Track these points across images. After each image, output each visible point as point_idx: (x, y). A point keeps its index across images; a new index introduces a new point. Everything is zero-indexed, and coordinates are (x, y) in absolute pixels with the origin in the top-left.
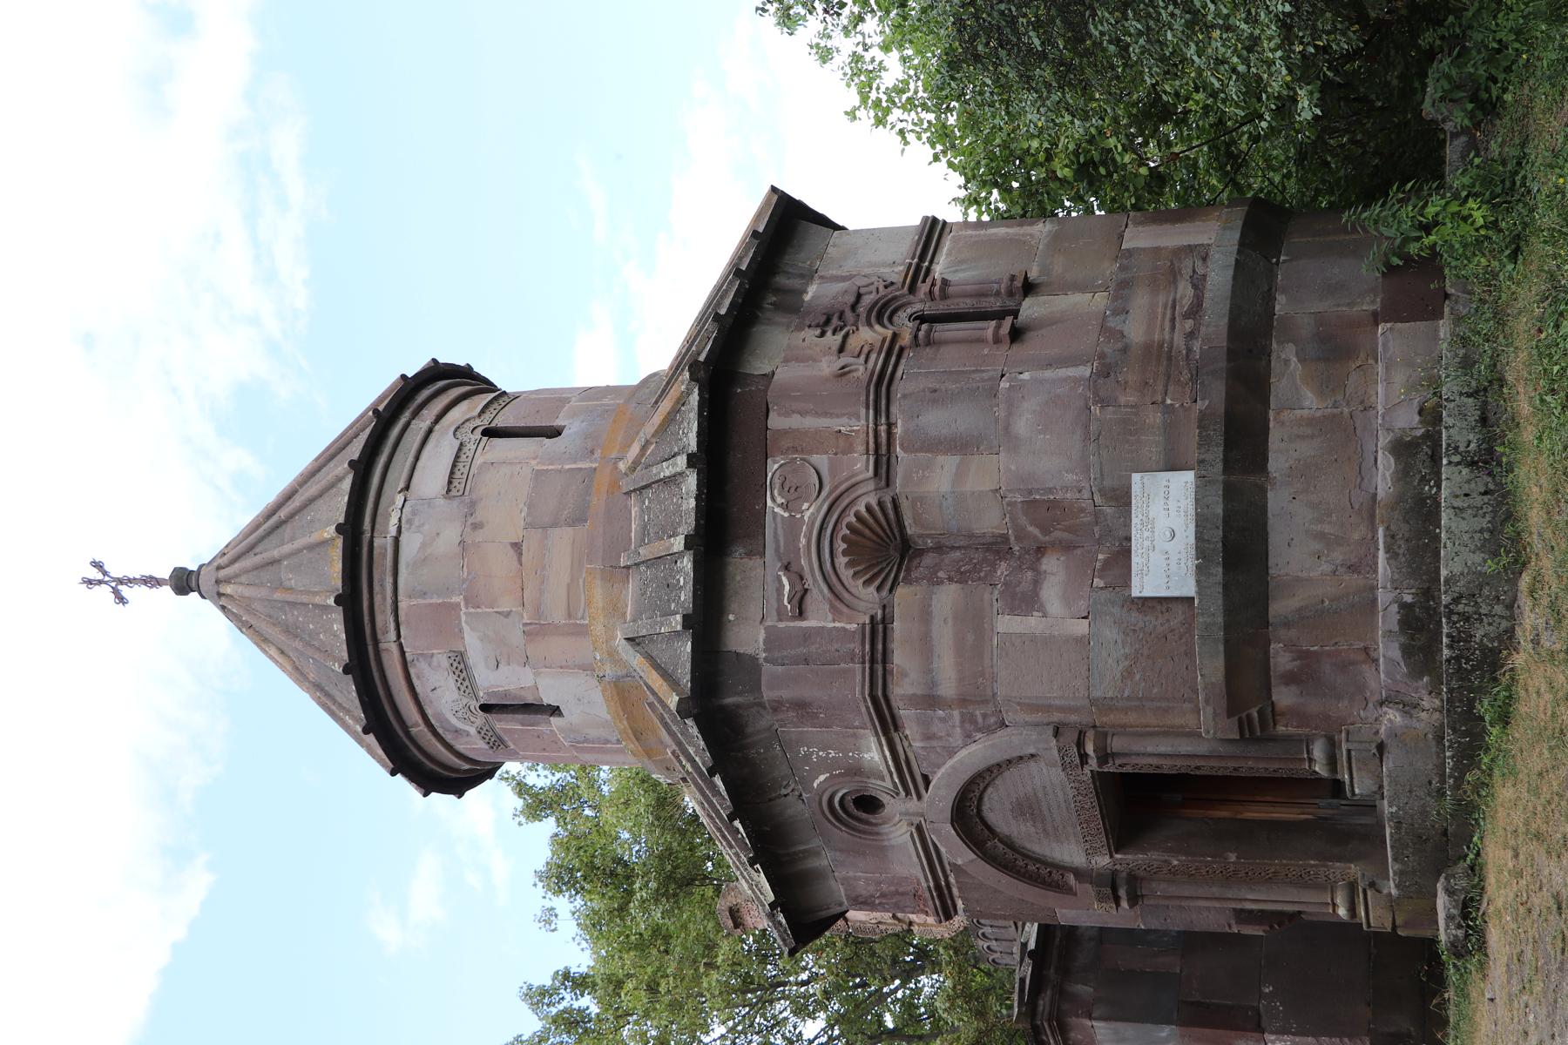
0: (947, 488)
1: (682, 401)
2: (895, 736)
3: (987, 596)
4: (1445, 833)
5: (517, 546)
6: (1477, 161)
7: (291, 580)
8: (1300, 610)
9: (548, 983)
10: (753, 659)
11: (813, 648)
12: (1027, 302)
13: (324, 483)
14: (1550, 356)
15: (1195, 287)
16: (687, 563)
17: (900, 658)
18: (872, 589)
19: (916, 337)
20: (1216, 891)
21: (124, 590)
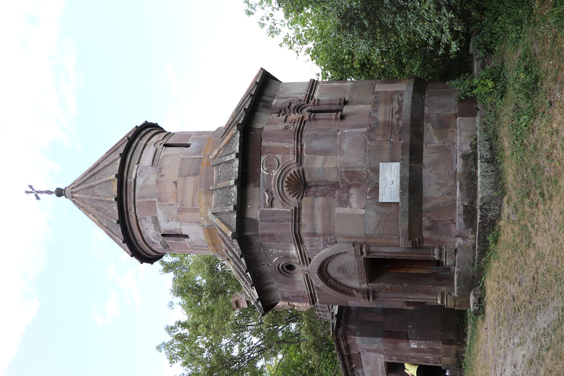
0: (318, 166)
1: (234, 136)
2: (301, 246)
3: (332, 201)
4: (474, 277)
5: (175, 183)
6: (488, 68)
7: (99, 192)
8: (432, 207)
9: (173, 325)
10: (256, 220)
11: (276, 217)
12: (345, 107)
13: (110, 161)
14: (517, 129)
15: (399, 104)
16: (235, 189)
17: (304, 221)
18: (295, 198)
19: (310, 117)
20: (400, 295)
21: (39, 195)
